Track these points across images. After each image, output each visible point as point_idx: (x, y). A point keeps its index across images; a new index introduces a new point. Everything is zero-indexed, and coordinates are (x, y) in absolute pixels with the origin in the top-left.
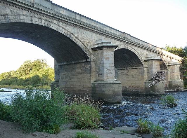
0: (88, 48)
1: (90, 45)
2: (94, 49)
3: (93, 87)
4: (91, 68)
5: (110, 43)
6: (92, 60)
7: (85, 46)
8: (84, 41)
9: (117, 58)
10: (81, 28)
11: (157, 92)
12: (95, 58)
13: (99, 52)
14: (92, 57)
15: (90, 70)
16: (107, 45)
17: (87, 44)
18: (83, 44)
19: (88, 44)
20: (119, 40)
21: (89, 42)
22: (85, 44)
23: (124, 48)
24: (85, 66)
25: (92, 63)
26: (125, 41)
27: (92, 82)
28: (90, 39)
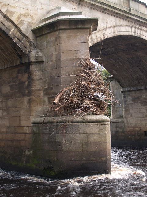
0: (23, 28)
1: (29, 23)
2: (39, 32)
3: (33, 133)
4: (30, 79)
5: (80, 13)
6: (33, 59)
7: (12, 23)
8: (12, 10)
9: (121, 62)
10: (129, 19)
11: (128, 127)
12: (40, 54)
13: (51, 38)
14: (33, 54)
15: (29, 86)
16: (70, 18)
17: (19, 18)
18: (5, 17)
19: (22, 18)
20: (116, 15)
21: (25, 15)
22: (14, 19)
23: (130, 34)
24: (20, 77)
25: (33, 68)
26: (131, 16)
27: (33, 119)
28: (30, 7)
